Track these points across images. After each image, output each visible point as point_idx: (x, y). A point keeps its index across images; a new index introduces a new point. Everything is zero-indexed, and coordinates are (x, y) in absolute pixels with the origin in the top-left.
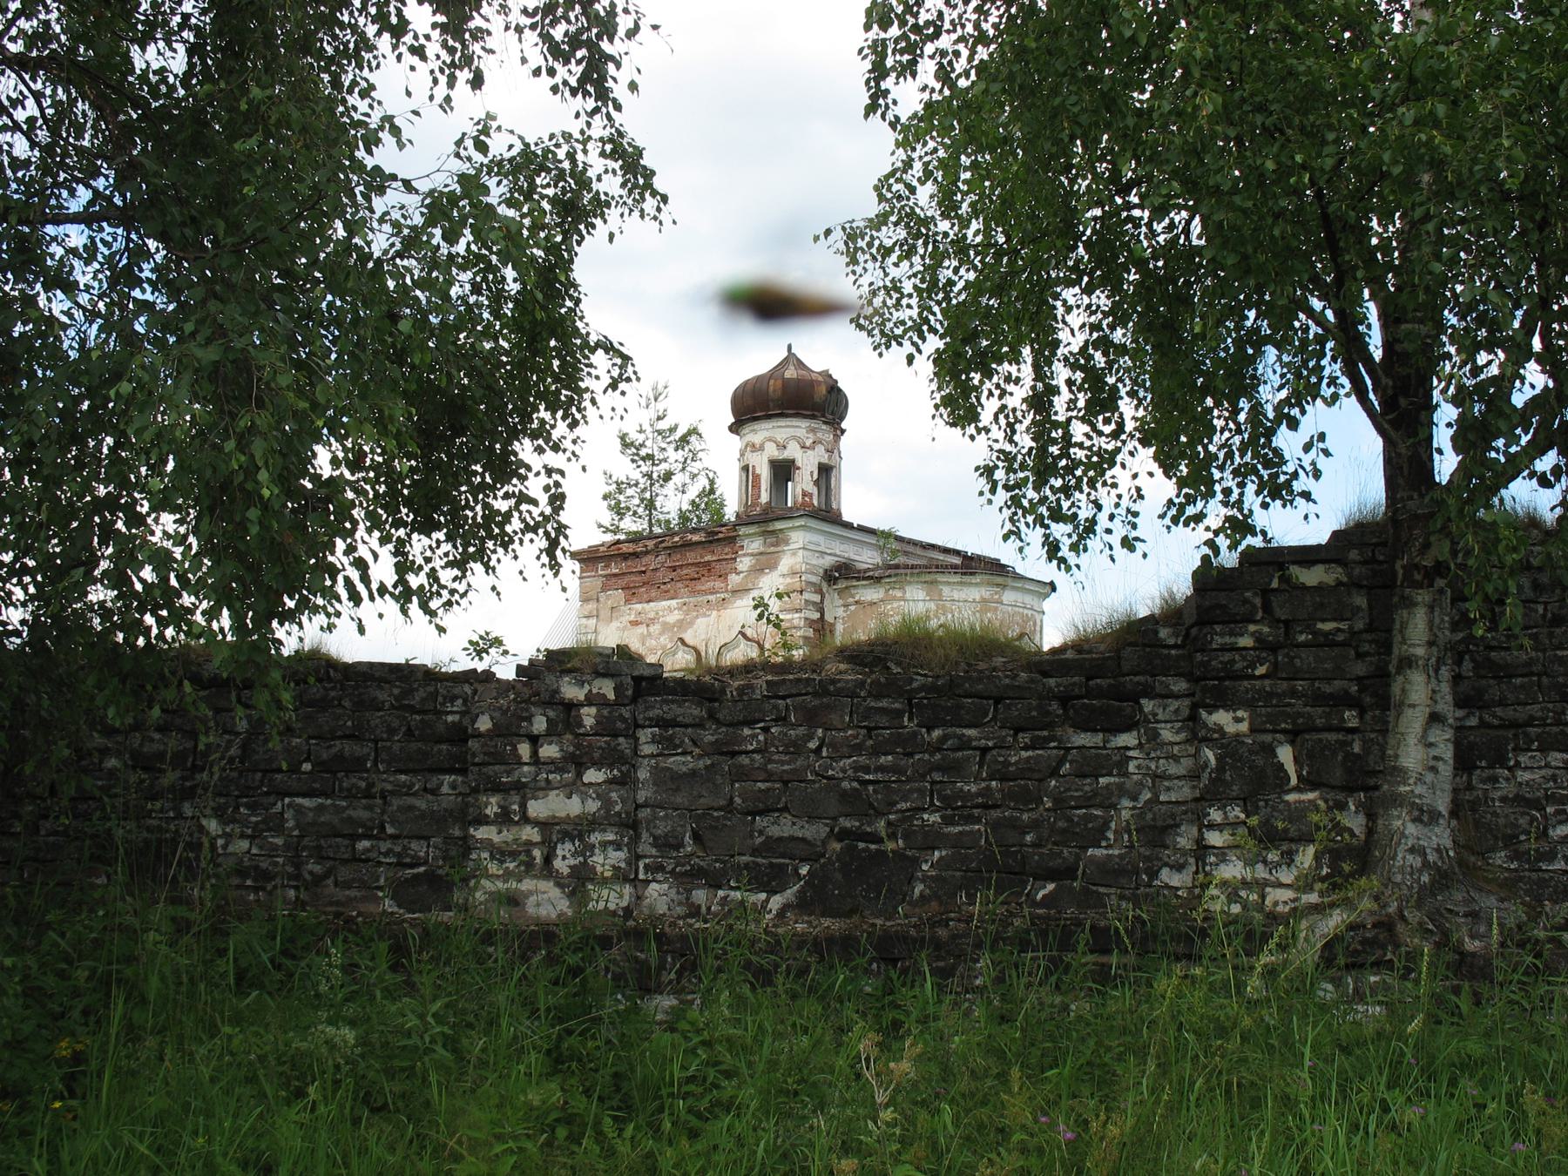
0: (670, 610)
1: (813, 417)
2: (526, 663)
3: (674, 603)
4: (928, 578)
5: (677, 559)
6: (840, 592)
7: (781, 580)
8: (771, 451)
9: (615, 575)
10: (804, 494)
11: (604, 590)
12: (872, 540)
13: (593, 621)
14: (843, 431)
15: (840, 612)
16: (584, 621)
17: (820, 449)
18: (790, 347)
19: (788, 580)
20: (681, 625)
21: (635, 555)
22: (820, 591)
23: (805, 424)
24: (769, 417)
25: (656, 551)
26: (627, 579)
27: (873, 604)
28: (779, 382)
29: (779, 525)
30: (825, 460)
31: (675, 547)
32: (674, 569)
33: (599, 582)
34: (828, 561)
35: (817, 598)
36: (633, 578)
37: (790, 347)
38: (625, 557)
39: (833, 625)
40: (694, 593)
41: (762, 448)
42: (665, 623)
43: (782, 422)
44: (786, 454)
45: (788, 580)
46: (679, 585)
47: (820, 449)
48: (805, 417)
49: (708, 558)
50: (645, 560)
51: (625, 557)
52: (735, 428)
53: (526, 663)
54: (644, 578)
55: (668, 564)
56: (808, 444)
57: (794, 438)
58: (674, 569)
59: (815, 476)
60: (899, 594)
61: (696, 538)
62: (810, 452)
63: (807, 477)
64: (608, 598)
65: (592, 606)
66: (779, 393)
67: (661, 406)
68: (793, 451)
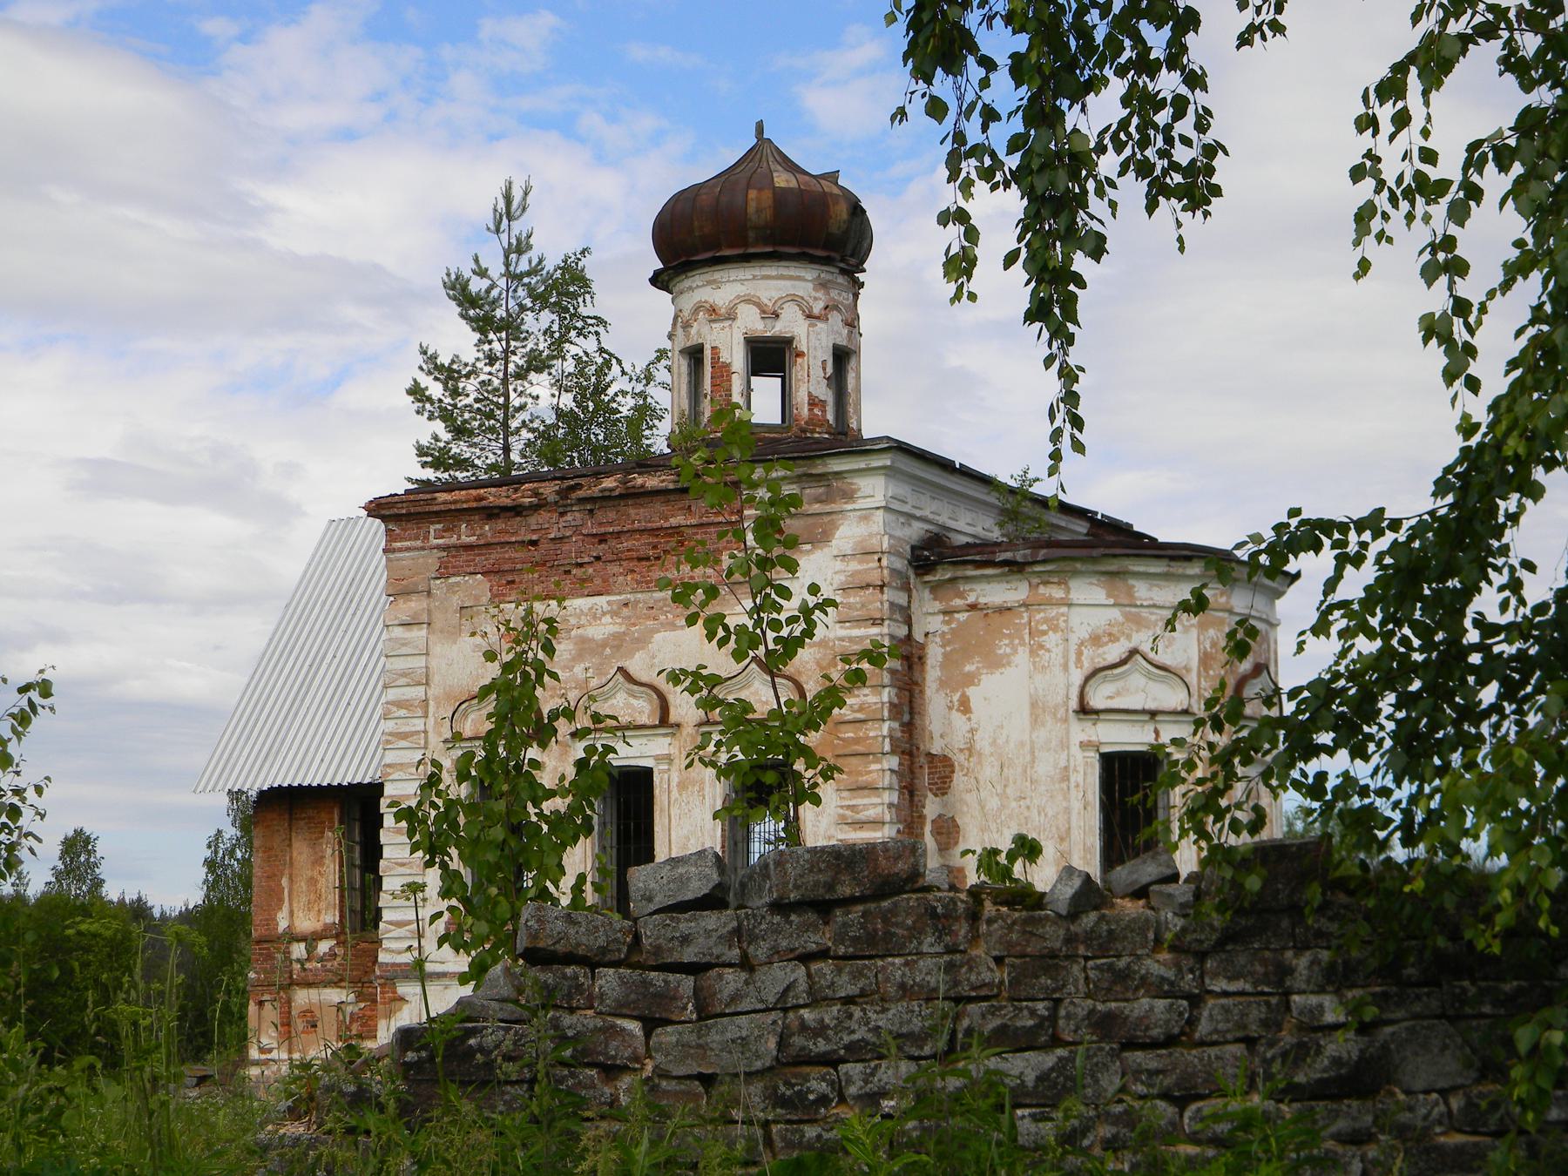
0: (595, 616)
1: (826, 261)
2: (1363, 595)
3: (601, 601)
4: (1113, 566)
5: (609, 519)
6: (935, 588)
7: (839, 565)
8: (750, 322)
9: (468, 547)
10: (814, 402)
11: (444, 572)
12: (992, 498)
13: (420, 633)
14: (862, 285)
15: (936, 623)
16: (398, 632)
17: (836, 319)
18: (760, 128)
19: (854, 566)
20: (617, 642)
21: (517, 511)
22: (906, 588)
23: (809, 273)
24: (746, 259)
25: (562, 505)
26: (495, 555)
27: (1004, 610)
28: (767, 196)
29: (836, 465)
30: (842, 341)
31: (606, 499)
32: (602, 539)
33: (432, 560)
34: (916, 531)
35: (901, 599)
36: (510, 553)
37: (760, 128)
38: (491, 513)
39: (922, 647)
40: (645, 584)
41: (731, 316)
42: (583, 640)
43: (771, 269)
44: (778, 329)
45: (854, 566)
46: (614, 568)
47: (836, 319)
48: (813, 260)
49: (677, 520)
50: (534, 521)
51: (491, 513)
52: (658, 281)
53: (1363, 595)
54: (536, 554)
55: (590, 527)
56: (816, 311)
57: (793, 299)
58: (602, 539)
59: (830, 370)
60: (1057, 593)
61: (652, 482)
62: (820, 325)
63: (817, 372)
64: (450, 588)
65: (415, 605)
66: (768, 215)
67: (518, 227)
68: (791, 324)
